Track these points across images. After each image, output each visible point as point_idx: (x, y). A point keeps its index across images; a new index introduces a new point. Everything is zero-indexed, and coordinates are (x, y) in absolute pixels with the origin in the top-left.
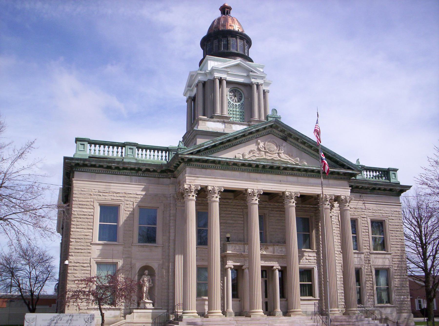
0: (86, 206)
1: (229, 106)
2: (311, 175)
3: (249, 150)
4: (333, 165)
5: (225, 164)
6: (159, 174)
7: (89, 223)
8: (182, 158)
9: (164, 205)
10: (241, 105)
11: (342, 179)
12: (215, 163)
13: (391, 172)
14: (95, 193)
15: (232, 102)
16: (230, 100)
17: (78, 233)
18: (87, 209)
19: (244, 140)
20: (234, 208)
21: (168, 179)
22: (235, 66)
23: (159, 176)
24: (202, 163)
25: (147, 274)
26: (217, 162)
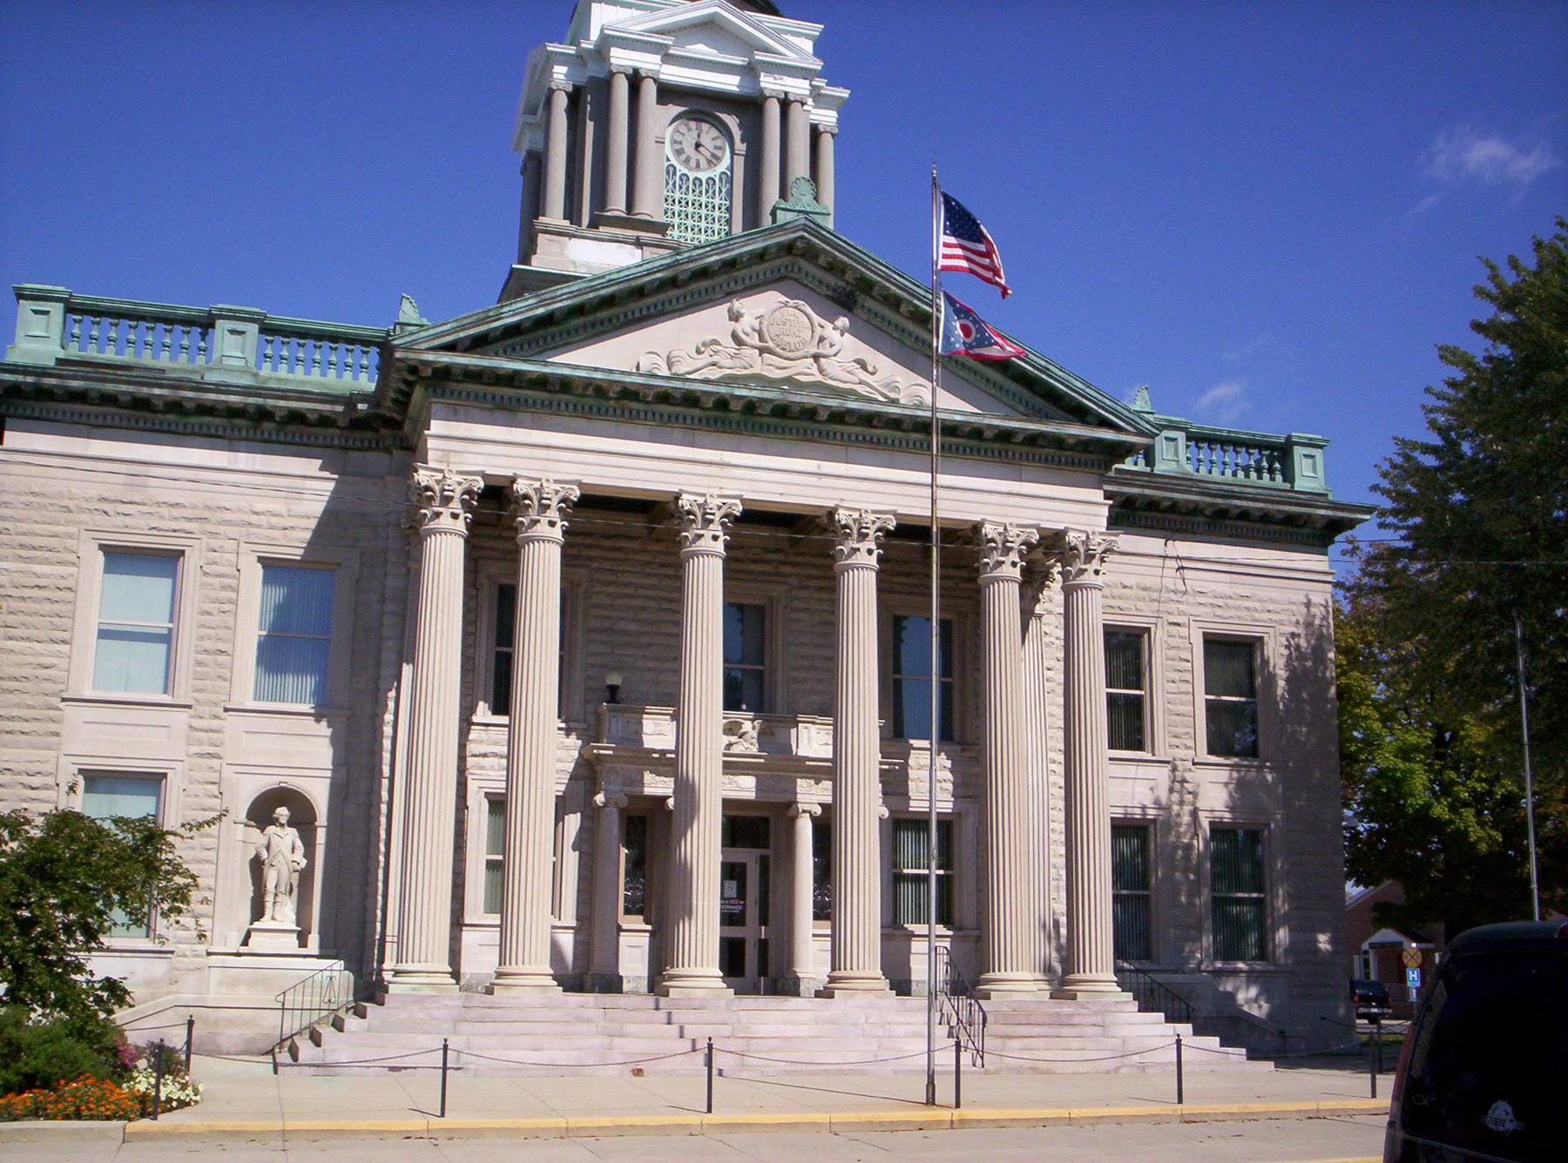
0: (48, 554)
1: (671, 183)
2: (954, 447)
3: (698, 340)
4: (1040, 410)
5: (590, 391)
6: (346, 433)
7: (56, 620)
8: (411, 363)
9: (362, 555)
10: (717, 179)
11: (1073, 463)
12: (548, 388)
13: (1298, 452)
14: (85, 505)
15: (681, 169)
16: (674, 161)
17: (12, 657)
18: (52, 564)
19: (674, 301)
20: (646, 575)
21: (384, 456)
22: (696, 26)
23: (347, 440)
24: (494, 385)
25: (283, 820)
26: (553, 385)
